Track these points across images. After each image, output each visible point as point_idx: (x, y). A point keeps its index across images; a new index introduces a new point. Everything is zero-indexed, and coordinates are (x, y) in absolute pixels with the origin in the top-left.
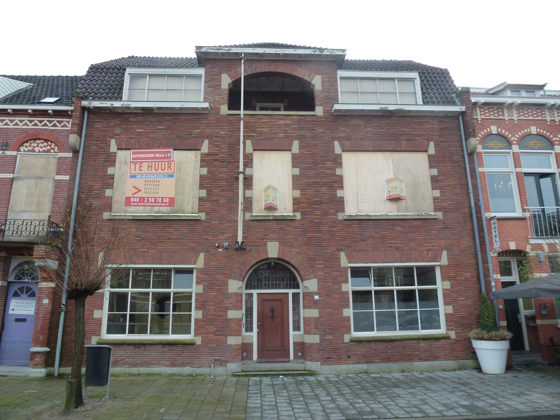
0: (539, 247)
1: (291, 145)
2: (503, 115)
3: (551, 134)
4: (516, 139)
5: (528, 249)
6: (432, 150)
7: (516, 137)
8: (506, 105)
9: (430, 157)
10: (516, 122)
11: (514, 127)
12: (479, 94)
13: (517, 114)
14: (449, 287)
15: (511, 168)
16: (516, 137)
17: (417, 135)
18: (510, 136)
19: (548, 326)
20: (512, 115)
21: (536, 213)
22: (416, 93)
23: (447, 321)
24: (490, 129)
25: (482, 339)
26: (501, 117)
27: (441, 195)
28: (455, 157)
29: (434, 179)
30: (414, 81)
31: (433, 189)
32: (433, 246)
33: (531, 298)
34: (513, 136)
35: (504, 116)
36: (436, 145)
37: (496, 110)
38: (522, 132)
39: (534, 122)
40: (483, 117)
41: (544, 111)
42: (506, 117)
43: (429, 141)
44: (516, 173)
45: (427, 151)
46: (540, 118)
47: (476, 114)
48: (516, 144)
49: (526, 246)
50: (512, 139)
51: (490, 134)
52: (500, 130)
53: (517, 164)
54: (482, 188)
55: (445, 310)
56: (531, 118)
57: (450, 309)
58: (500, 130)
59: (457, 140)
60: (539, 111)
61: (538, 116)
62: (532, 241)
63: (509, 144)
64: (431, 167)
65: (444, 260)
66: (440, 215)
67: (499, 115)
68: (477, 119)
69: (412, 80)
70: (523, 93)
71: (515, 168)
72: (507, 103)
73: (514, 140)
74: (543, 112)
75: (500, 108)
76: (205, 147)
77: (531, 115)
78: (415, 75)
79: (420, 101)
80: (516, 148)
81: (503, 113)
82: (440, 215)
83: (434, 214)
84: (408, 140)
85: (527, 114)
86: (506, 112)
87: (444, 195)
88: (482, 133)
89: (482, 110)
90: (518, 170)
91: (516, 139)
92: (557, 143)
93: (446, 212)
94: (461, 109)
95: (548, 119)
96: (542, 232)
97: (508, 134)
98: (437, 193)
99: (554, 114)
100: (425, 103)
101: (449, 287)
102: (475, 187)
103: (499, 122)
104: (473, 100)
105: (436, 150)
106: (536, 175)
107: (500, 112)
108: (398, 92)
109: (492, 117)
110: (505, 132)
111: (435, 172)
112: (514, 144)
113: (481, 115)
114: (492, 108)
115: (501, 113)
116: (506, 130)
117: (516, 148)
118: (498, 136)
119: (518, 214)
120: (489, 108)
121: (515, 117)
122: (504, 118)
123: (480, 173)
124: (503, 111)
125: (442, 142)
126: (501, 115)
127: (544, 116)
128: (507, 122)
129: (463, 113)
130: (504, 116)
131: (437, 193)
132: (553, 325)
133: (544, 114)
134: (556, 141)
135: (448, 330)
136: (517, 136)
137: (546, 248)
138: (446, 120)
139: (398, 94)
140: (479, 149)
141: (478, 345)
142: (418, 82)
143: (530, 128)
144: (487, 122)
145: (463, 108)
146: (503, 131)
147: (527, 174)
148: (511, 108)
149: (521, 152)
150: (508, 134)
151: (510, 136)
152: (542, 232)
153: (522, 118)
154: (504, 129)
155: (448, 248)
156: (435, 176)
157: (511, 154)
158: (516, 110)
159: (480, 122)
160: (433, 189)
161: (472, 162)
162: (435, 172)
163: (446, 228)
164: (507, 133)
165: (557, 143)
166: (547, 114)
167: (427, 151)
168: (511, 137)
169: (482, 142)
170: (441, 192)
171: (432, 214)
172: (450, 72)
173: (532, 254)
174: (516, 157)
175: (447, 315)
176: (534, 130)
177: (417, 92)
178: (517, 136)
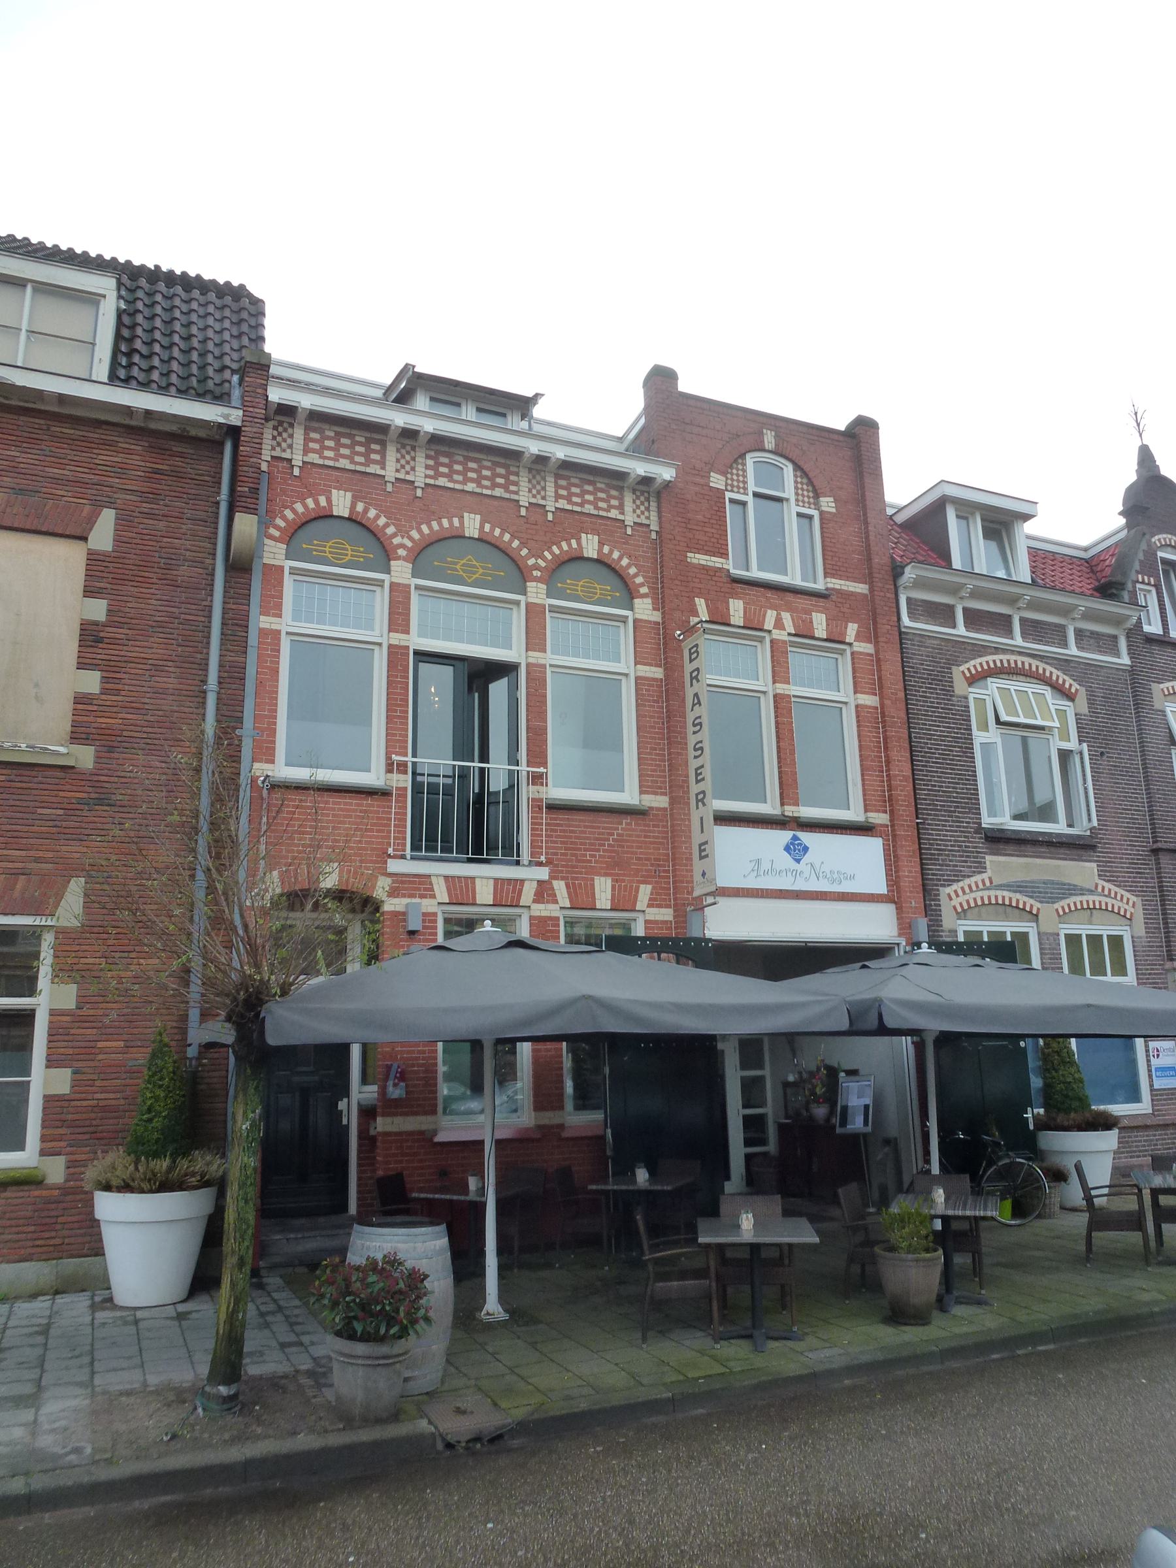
0: (419, 886)
1: (91, 521)
2: (382, 464)
3: (523, 544)
4: (409, 544)
5: (381, 888)
6: (103, 535)
7: (410, 538)
8: (631, 479)
9: (95, 560)
10: (419, 493)
11: (411, 503)
12: (293, 384)
13: (427, 467)
14: (72, 1005)
15: (378, 631)
16: (410, 538)
17: (56, 481)
18: (391, 530)
19: (401, 1137)
20: (413, 469)
21: (441, 780)
22: (93, 344)
23: (47, 1122)
24: (329, 501)
25: (126, 1187)
26: (373, 469)
27: (104, 691)
28: (184, 572)
29: (90, 635)
30: (97, 304)
31: (81, 665)
32: (37, 860)
33: (513, 1041)
34: (402, 531)
35: (383, 468)
36: (123, 523)
37: (360, 444)
38: (555, 548)
39: (478, 502)
40: (562, 504)
41: (517, 474)
42: (390, 473)
43: (98, 506)
44: (390, 646)
45: (84, 539)
46: (498, 492)
47: (290, 446)
48: (405, 559)
49: (373, 879)
50: (397, 541)
51: (326, 516)
52: (360, 507)
53: (399, 619)
54: (260, 684)
55: (46, 1082)
56: (470, 487)
57: (62, 1082)
58: (606, 549)
59: (202, 515)
60: (501, 471)
61: (495, 486)
62: (394, 866)
63: (385, 555)
64: (89, 592)
65: (71, 908)
66: (85, 757)
67: (369, 462)
68: (290, 460)
69: (92, 299)
70: (469, 412)
71: (855, 693)
72: (659, 481)
73: (402, 546)
74: (512, 478)
75: (377, 442)
76: (103, 533)
77: (472, 480)
78: (106, 285)
79: (102, 371)
80: (401, 571)
81: (384, 457)
82: (85, 757)
83: (62, 750)
84: (21, 491)
85: (581, 495)
86: (392, 454)
87: (117, 692)
88: (299, 508)
89: (563, 483)
90: (781, 688)
91: (409, 544)
92: (536, 573)
93: (111, 749)
94: (226, 416)
95: (524, 499)
96: (446, 839)
97: (387, 525)
98: (91, 682)
99: (544, 488)
100: (113, 378)
101: (72, 1005)
102: (233, 675)
103: (608, 529)
104: (276, 395)
105: (117, 540)
106: (458, 664)
107: (375, 452)
108: (24, 327)
109: (344, 463)
110: (377, 517)
111: (98, 610)
112: (398, 558)
113: (558, 497)
114: (350, 436)
115: (614, 502)
116: (382, 511)
117: (401, 571)
118: (348, 524)
119: (373, 778)
120: (369, 441)
121: (420, 475)
122: (382, 473)
123: (263, 633)
124: (621, 499)
125: (150, 515)
126: (375, 462)
127: (512, 488)
128: (389, 488)
129: (234, 432)
130: (383, 468)
131: (91, 682)
132: (422, 1133)
133: (516, 484)
134: (536, 567)
135: (43, 1153)
136: (415, 534)
137: (442, 893)
138: (178, 448)
139: (23, 335)
140: (274, 553)
141: (111, 1208)
142: (109, 307)
143: (579, 540)
144: (314, 479)
145: (235, 417)
146: (372, 513)
147: (423, 656)
148: (414, 448)
149: (554, 609)
150: (387, 525)
151: (391, 530)
152: (446, 839)
153: (442, 482)
154: (376, 507)
155: (89, 872)
156: (96, 623)
157: (387, 585)
158: (428, 457)
159: (296, 472)
160: (81, 665)
161: (238, 592)
162: (98, 610)
163: (100, 802)
164: (625, 562)
165: (536, 573)
166: (524, 484)
167: (84, 539)
168: (394, 535)
169: (291, 535)
170: (105, 680)
171: (61, 750)
172: (268, 310)
173: (391, 905)
174: (535, 615)
175: (50, 1101)
176: (472, 525)
177: (97, 341)
178: (415, 534)
